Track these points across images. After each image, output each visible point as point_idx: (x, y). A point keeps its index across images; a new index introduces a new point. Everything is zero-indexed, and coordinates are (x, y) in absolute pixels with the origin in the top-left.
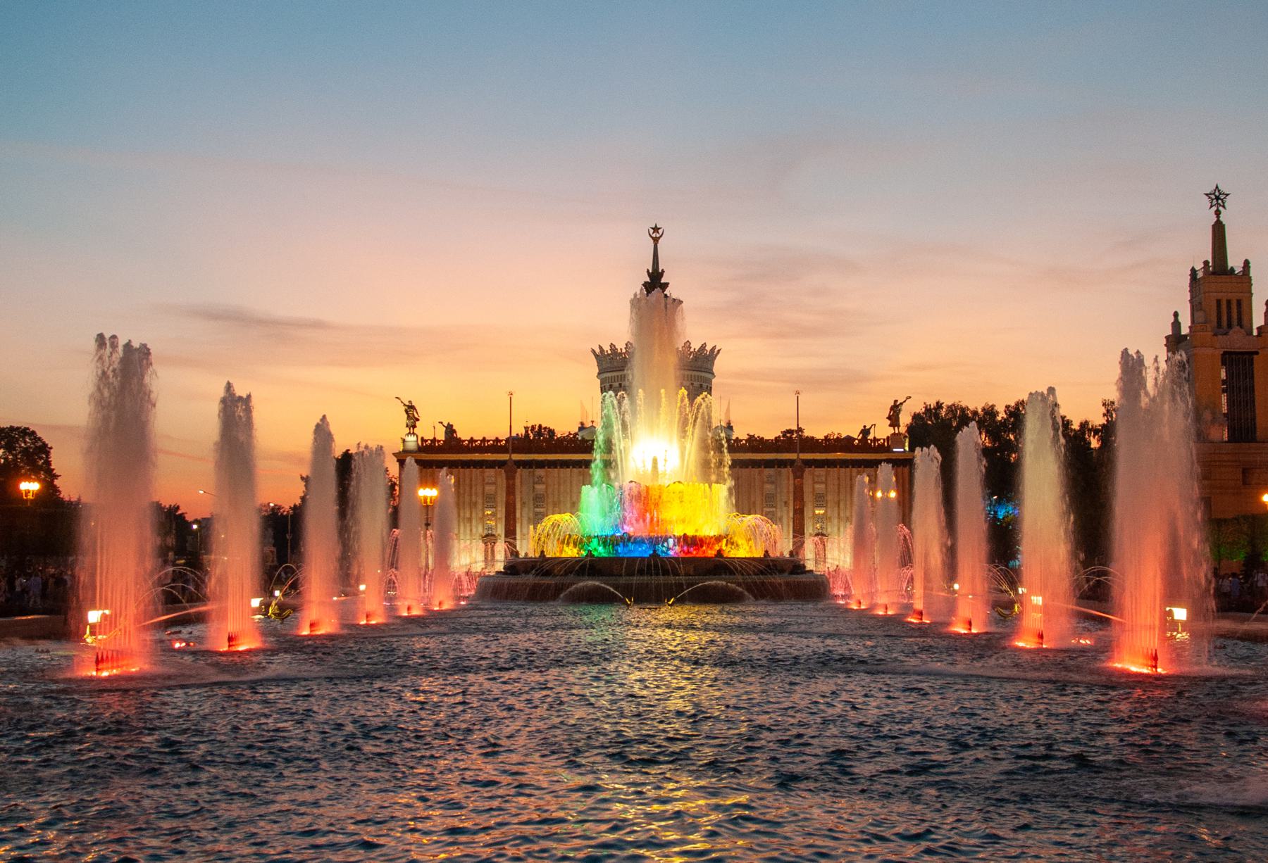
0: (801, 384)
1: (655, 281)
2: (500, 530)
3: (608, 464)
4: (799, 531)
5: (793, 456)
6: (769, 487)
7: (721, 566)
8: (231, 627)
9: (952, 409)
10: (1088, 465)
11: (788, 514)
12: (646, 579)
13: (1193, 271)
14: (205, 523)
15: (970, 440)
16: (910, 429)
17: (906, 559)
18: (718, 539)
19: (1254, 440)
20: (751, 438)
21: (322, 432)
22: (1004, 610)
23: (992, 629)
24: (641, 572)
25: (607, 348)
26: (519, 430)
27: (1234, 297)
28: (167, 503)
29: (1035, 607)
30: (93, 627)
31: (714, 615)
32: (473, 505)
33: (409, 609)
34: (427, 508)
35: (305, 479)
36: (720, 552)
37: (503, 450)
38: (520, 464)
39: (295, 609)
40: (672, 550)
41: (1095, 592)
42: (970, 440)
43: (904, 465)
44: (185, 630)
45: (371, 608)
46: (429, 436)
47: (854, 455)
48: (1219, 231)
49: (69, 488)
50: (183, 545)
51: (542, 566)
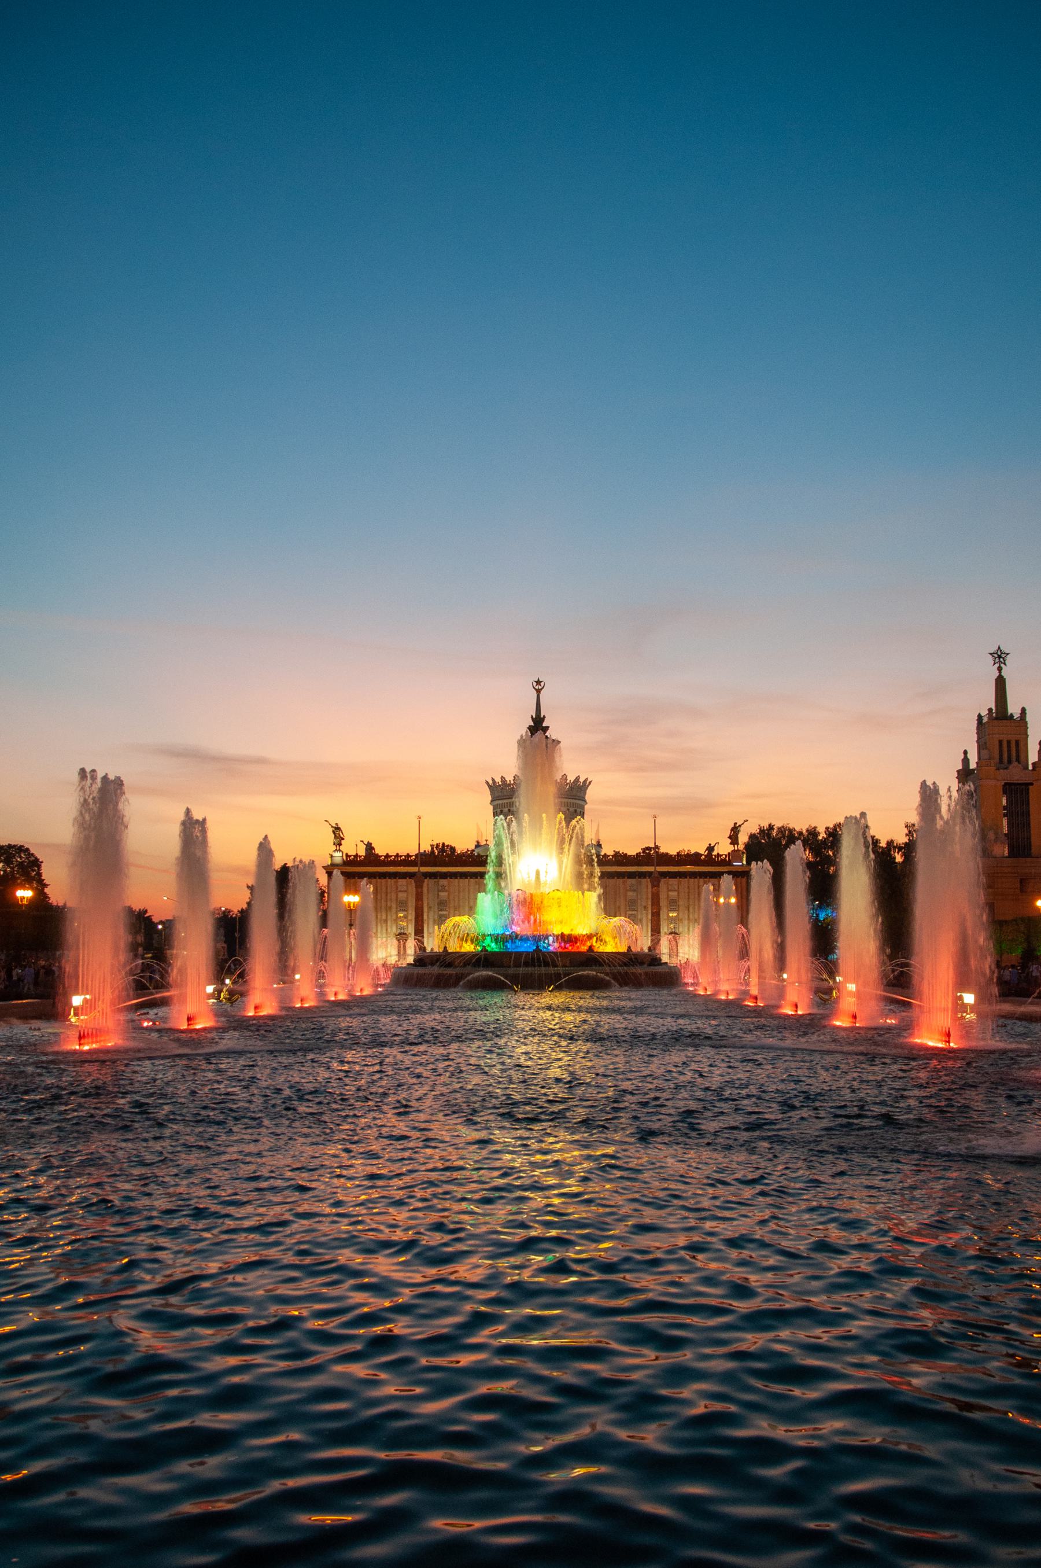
0: (657, 809)
1: (538, 725)
2: (411, 930)
3: (499, 875)
4: (656, 930)
5: (651, 869)
7: (592, 959)
8: (190, 1009)
9: (782, 830)
10: (894, 876)
11: (647, 917)
12: (530, 969)
14: (169, 924)
15: (796, 856)
16: (747, 846)
17: (744, 953)
18: (590, 937)
19: (1029, 856)
20: (617, 854)
21: (265, 849)
22: (824, 995)
24: (526, 964)
25: (498, 780)
26: (426, 847)
27: (1013, 738)
28: (137, 907)
29: (850, 993)
30: (76, 1009)
31: (586, 999)
32: (388, 909)
34: (351, 911)
36: (591, 948)
37: (413, 863)
38: (427, 875)
39: (242, 994)
41: (899, 980)
42: (796, 856)
43: (742, 876)
44: (152, 1012)
45: (305, 994)
46: (352, 853)
47: (702, 867)
48: (1000, 684)
49: (56, 895)
50: (150, 942)
51: (445, 959)
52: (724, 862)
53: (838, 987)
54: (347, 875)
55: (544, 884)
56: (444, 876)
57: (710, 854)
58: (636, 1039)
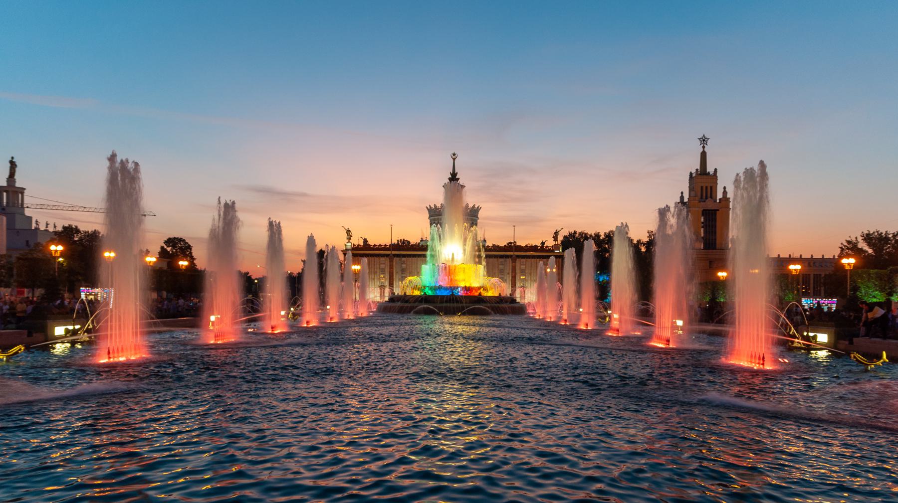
0: (515, 223)
1: (454, 177)
2: (387, 284)
3: (433, 256)
4: (514, 285)
5: (512, 253)
6: (501, 267)
7: (480, 299)
8: (273, 323)
9: (581, 234)
10: (644, 258)
11: (509, 278)
12: (448, 304)
13: (691, 174)
14: (262, 280)
15: (590, 248)
16: (562, 242)
17: (560, 297)
18: (479, 288)
19: (715, 248)
20: (494, 245)
21: (311, 241)
22: (602, 319)
23: (596, 327)
24: (446, 302)
25: (433, 206)
26: (395, 241)
27: (709, 185)
28: (244, 271)
29: (615, 319)
30: (213, 322)
31: (477, 320)
32: (375, 273)
33: (308, 322)
34: (356, 274)
35: (304, 261)
36: (480, 294)
37: (388, 249)
38: (395, 255)
39: (300, 315)
40: (460, 293)
41: (645, 312)
42: (590, 248)
43: (560, 258)
44: (252, 325)
45: (333, 314)
46: (356, 243)
47: (539, 253)
48: (704, 155)
49: (200, 264)
50: (252, 289)
51: (405, 299)
52: (551, 250)
53: (610, 316)
54: (354, 255)
55: (454, 260)
56: (404, 256)
57: (542, 246)
58: (501, 340)
